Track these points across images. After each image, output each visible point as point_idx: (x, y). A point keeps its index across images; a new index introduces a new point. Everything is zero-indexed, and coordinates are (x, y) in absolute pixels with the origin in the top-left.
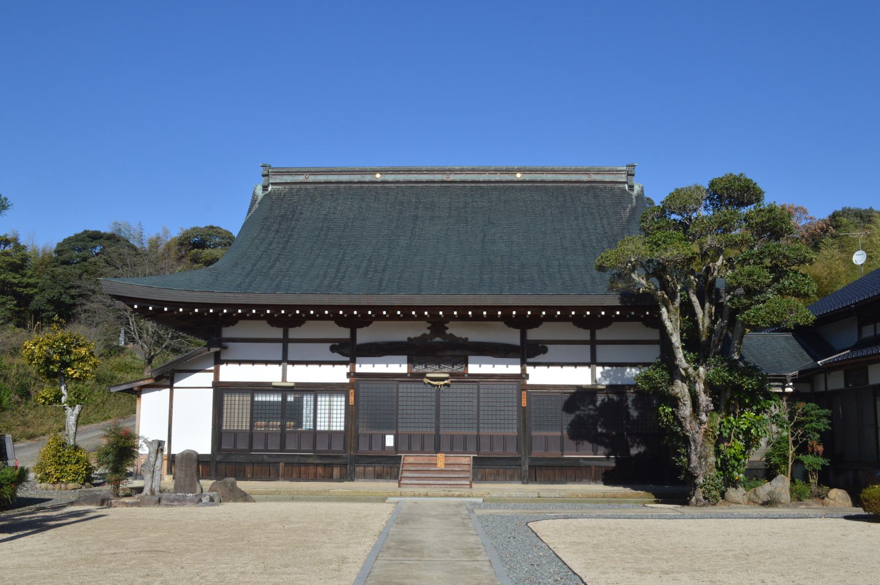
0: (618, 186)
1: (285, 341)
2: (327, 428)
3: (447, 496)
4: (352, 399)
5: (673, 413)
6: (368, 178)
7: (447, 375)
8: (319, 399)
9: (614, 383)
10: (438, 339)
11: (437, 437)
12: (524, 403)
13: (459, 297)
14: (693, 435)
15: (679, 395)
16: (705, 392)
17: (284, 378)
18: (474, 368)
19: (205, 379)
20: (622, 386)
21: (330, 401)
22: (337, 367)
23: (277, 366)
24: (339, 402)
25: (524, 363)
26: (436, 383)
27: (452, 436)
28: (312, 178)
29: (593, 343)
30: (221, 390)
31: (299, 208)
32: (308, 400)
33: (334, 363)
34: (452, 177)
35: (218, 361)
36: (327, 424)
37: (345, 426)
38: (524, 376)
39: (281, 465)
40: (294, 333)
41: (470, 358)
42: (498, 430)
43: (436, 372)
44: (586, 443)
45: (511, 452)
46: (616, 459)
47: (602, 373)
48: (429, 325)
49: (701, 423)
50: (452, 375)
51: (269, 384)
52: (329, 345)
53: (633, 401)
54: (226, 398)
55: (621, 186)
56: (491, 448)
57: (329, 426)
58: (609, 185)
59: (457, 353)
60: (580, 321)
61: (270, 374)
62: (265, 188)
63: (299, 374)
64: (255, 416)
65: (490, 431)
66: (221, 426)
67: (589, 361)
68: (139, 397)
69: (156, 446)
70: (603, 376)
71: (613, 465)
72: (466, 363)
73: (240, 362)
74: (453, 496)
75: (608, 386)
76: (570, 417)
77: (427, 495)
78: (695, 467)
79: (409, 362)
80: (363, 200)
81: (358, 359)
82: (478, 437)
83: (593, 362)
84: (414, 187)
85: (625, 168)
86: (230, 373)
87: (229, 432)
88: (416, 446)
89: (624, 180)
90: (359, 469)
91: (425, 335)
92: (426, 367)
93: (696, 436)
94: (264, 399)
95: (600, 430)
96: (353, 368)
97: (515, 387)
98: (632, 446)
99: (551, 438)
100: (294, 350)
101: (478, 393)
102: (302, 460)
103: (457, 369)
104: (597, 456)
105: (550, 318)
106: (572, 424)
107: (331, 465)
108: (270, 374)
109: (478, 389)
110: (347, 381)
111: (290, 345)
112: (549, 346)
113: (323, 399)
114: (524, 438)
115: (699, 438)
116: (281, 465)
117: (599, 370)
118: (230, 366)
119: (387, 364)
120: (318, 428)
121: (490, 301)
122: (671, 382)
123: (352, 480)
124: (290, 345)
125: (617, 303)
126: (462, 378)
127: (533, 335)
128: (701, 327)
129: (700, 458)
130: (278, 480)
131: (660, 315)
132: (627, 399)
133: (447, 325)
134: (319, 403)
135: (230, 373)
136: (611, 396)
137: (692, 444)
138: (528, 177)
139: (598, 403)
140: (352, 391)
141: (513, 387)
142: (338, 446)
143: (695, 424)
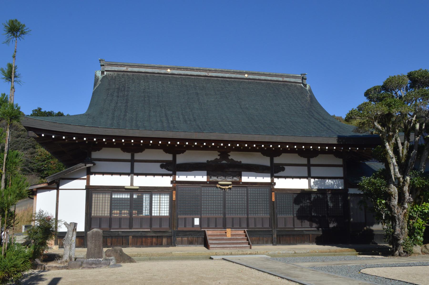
0: (298, 84)
1: (132, 161)
2: (158, 215)
3: (243, 254)
4: (174, 197)
5: (386, 203)
6: (163, 71)
7: (231, 183)
8: (153, 196)
9: (320, 188)
10: (224, 162)
11: (225, 219)
12: (273, 199)
13: (250, 136)
14: (398, 215)
15: (393, 193)
16: (408, 191)
17: (132, 184)
18: (245, 179)
19: (81, 184)
20: (325, 190)
21: (160, 198)
22: (165, 177)
23: (127, 176)
24: (165, 199)
25: (272, 177)
26: (224, 187)
27: (233, 219)
28: (130, 69)
29: (309, 166)
30: (90, 190)
31: (127, 85)
32: (146, 197)
33: (163, 175)
34: (210, 74)
35: (89, 172)
36: (158, 212)
37: (170, 213)
38: (273, 184)
39: (130, 237)
40: (138, 156)
41: (243, 173)
42: (212, 215)
43: (225, 181)
44: (306, 221)
46: (323, 230)
47: (314, 182)
48: (219, 153)
49: (404, 208)
50: (233, 183)
51: (123, 187)
52: (159, 164)
53: (330, 197)
54: (94, 196)
55: (299, 84)
56: (185, 226)
57: (160, 213)
58: (293, 84)
59: (236, 170)
60: (301, 153)
61: (123, 181)
62: (103, 73)
63: (141, 181)
64: (113, 207)
65: (207, 215)
66: (91, 213)
67: (307, 175)
68: (36, 195)
69: (72, 227)
70: (314, 184)
71: (321, 233)
72: (240, 176)
73: (103, 174)
74: (247, 254)
75: (318, 190)
76: (297, 207)
77: (231, 254)
78: (398, 234)
79: (208, 175)
80: (163, 83)
81: (177, 173)
83: (309, 176)
84: (190, 78)
85: (300, 76)
86: (96, 180)
87: (96, 218)
88: (212, 225)
89: (301, 81)
90: (179, 239)
91: (216, 159)
92: (217, 177)
93: (400, 216)
94: (119, 197)
95: (313, 214)
96: (175, 178)
97: (268, 190)
98: (330, 223)
99: (287, 219)
100: (138, 167)
101: (247, 193)
102: (143, 234)
103: (236, 179)
106: (299, 211)
107: (162, 237)
108: (123, 181)
109: (247, 191)
110: (171, 186)
111: (136, 164)
112: (286, 167)
113: (156, 196)
114: (273, 220)
115: (401, 217)
116: (130, 237)
117: (312, 180)
118: (97, 176)
119: (195, 176)
120: (153, 214)
122: (388, 185)
123: (175, 246)
124: (136, 164)
125: (335, 142)
126: (238, 184)
128: (401, 155)
129: (401, 229)
130: (129, 247)
131: (385, 147)
132: (327, 197)
133: (229, 154)
134: (153, 199)
135: (96, 180)
136: (319, 195)
137: (397, 221)
138: (251, 77)
139: (312, 199)
140: (174, 192)
141: (267, 190)
142: (165, 226)
143: (400, 210)
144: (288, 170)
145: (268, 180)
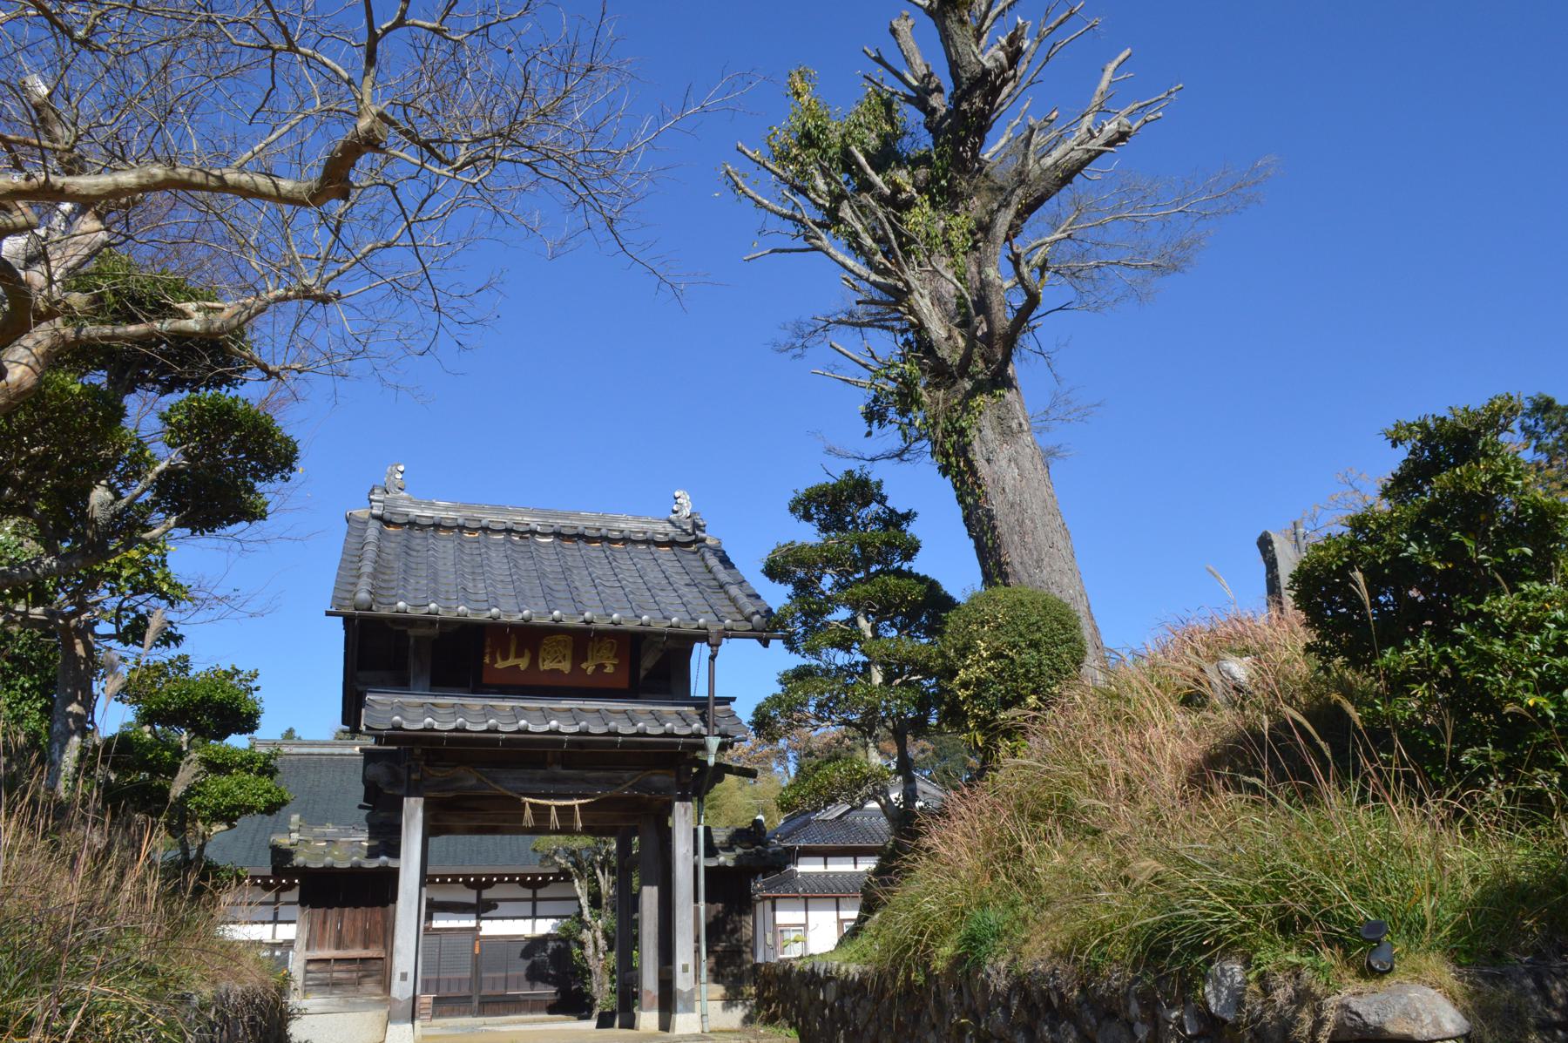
1: (534, 900)
17: (274, 937)
25: (479, 918)
45: (465, 992)
82: (438, 981)
104: (548, 991)
105: (501, 881)
115: (598, 970)
121: (454, 871)
127: (487, 894)
144: (503, 908)
145: (473, 924)
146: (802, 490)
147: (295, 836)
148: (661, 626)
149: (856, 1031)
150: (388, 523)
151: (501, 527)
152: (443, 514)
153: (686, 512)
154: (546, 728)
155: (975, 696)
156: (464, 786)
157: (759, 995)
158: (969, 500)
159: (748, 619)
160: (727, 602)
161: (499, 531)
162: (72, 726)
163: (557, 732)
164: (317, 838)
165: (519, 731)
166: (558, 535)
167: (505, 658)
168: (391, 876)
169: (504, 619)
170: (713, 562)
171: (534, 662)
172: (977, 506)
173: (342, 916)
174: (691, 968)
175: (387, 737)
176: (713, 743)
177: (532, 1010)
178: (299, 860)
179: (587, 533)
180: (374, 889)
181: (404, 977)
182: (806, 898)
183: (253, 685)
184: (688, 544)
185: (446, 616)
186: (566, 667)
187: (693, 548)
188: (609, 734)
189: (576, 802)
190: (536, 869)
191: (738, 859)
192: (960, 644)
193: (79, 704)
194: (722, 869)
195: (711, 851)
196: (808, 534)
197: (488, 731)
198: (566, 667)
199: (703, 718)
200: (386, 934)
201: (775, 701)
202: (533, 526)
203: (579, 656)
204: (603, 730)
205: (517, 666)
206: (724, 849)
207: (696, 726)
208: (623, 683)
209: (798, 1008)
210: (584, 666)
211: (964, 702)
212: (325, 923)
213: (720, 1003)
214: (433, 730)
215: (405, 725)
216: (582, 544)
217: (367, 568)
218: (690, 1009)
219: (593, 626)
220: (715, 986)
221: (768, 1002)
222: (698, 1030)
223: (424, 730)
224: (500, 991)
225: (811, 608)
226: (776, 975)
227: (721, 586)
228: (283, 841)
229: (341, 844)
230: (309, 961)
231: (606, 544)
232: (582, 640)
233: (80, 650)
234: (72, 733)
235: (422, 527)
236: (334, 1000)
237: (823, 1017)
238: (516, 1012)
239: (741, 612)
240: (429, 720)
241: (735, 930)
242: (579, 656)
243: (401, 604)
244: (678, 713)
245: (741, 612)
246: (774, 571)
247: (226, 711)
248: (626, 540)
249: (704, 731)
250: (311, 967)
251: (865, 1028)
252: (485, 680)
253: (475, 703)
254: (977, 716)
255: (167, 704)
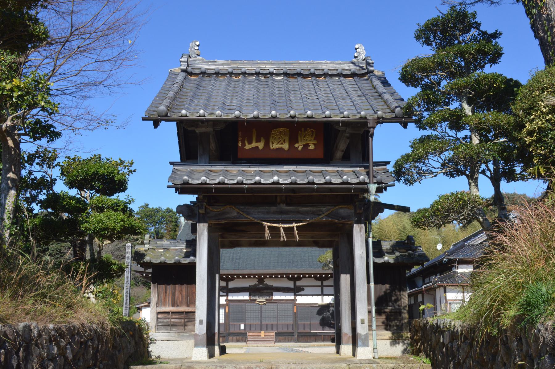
1: (322, 286)
25: (295, 295)
45: (290, 330)
82: (277, 325)
105: (304, 277)
127: (299, 283)
145: (292, 298)
146: (422, 23)
147: (147, 246)
148: (337, 117)
149: (459, 362)
150: (191, 74)
151: (254, 72)
152: (221, 67)
153: (363, 56)
154: (271, 181)
155: (539, 141)
156: (229, 217)
157: (412, 338)
158: (534, 11)
159: (393, 111)
160: (383, 103)
161: (252, 75)
162: (10, 185)
163: (278, 183)
164: (159, 247)
165: (255, 183)
166: (286, 74)
167: (250, 143)
168: (192, 267)
169: (243, 117)
170: (377, 82)
171: (267, 144)
172: (540, 14)
173: (174, 289)
174: (366, 321)
175: (181, 188)
176: (373, 187)
177: (324, 340)
178: (147, 259)
179: (302, 72)
180: (183, 274)
181: (201, 322)
182: (463, 286)
183: (132, 169)
184: (363, 75)
185: (209, 117)
186: (286, 146)
187: (367, 77)
188: (309, 183)
189: (294, 225)
190: (321, 271)
191: (397, 259)
192: (526, 106)
193: (13, 173)
194: (386, 264)
195: (379, 252)
196: (427, 52)
197: (237, 183)
198: (286, 146)
199: (368, 174)
200: (191, 300)
201: (407, 157)
202: (271, 70)
203: (293, 140)
204: (305, 181)
205: (257, 147)
206: (388, 253)
207: (362, 177)
208: (320, 154)
209: (431, 346)
210: (296, 145)
211: (529, 145)
212: (166, 292)
213: (389, 342)
214: (206, 184)
215: (191, 181)
216: (299, 79)
217: (171, 94)
218: (366, 345)
219: (295, 119)
220: (386, 332)
221: (417, 342)
222: (371, 357)
223: (201, 184)
224: (307, 330)
225: (431, 97)
226: (420, 326)
227: (380, 96)
228: (142, 249)
229: (169, 252)
230: (159, 313)
231: (314, 78)
232: (294, 128)
233: (11, 143)
234: (10, 188)
235: (209, 75)
236: (172, 334)
237: (442, 352)
238: (316, 341)
239: (389, 107)
240: (204, 178)
241: (397, 300)
242: (293, 140)
243: (184, 112)
244: (354, 171)
245: (389, 107)
246: (408, 78)
247: (109, 181)
248: (326, 75)
249: (367, 181)
250: (160, 316)
251: (464, 361)
252: (240, 155)
253: (234, 169)
254: (540, 154)
255: (77, 176)
